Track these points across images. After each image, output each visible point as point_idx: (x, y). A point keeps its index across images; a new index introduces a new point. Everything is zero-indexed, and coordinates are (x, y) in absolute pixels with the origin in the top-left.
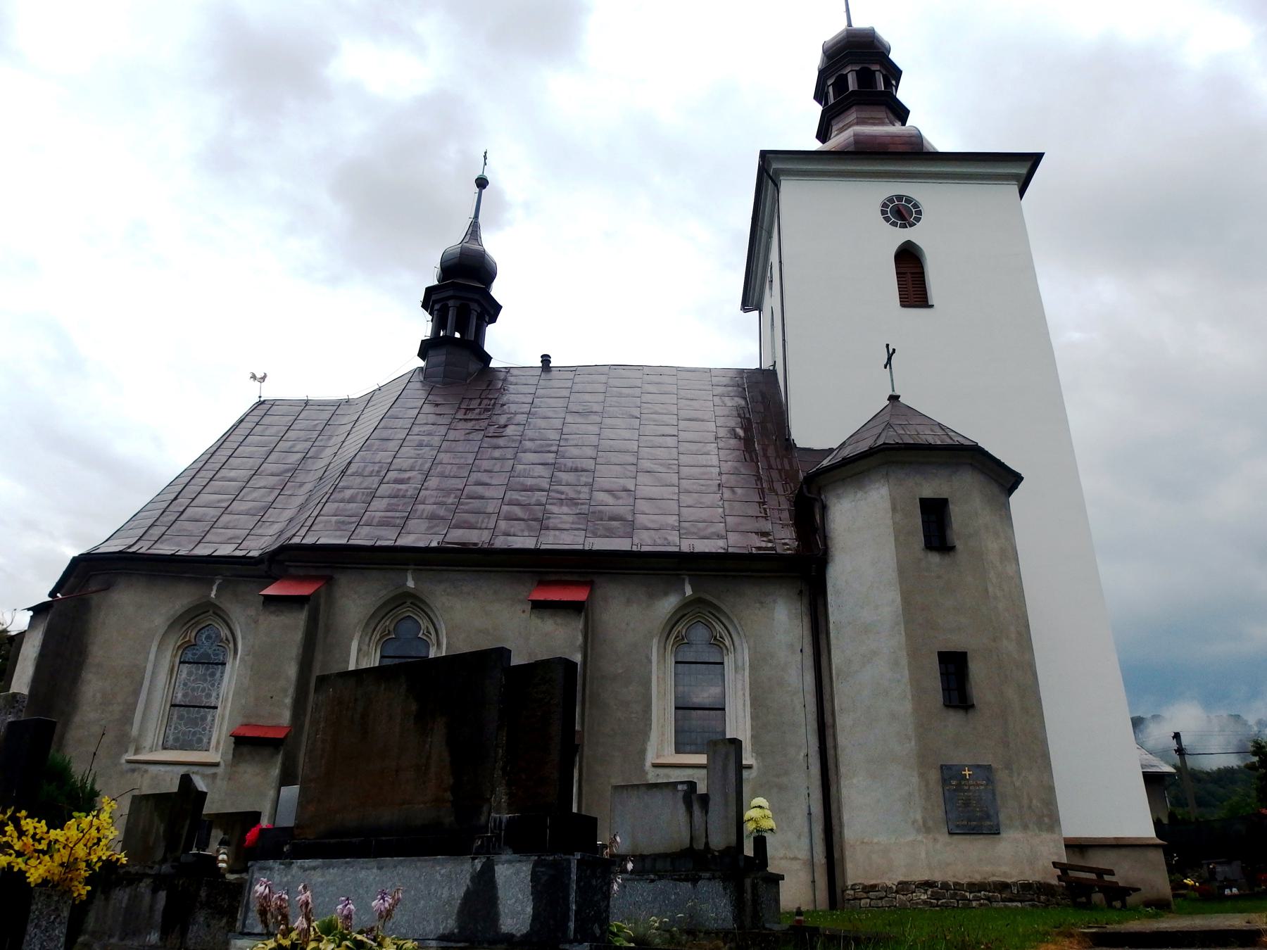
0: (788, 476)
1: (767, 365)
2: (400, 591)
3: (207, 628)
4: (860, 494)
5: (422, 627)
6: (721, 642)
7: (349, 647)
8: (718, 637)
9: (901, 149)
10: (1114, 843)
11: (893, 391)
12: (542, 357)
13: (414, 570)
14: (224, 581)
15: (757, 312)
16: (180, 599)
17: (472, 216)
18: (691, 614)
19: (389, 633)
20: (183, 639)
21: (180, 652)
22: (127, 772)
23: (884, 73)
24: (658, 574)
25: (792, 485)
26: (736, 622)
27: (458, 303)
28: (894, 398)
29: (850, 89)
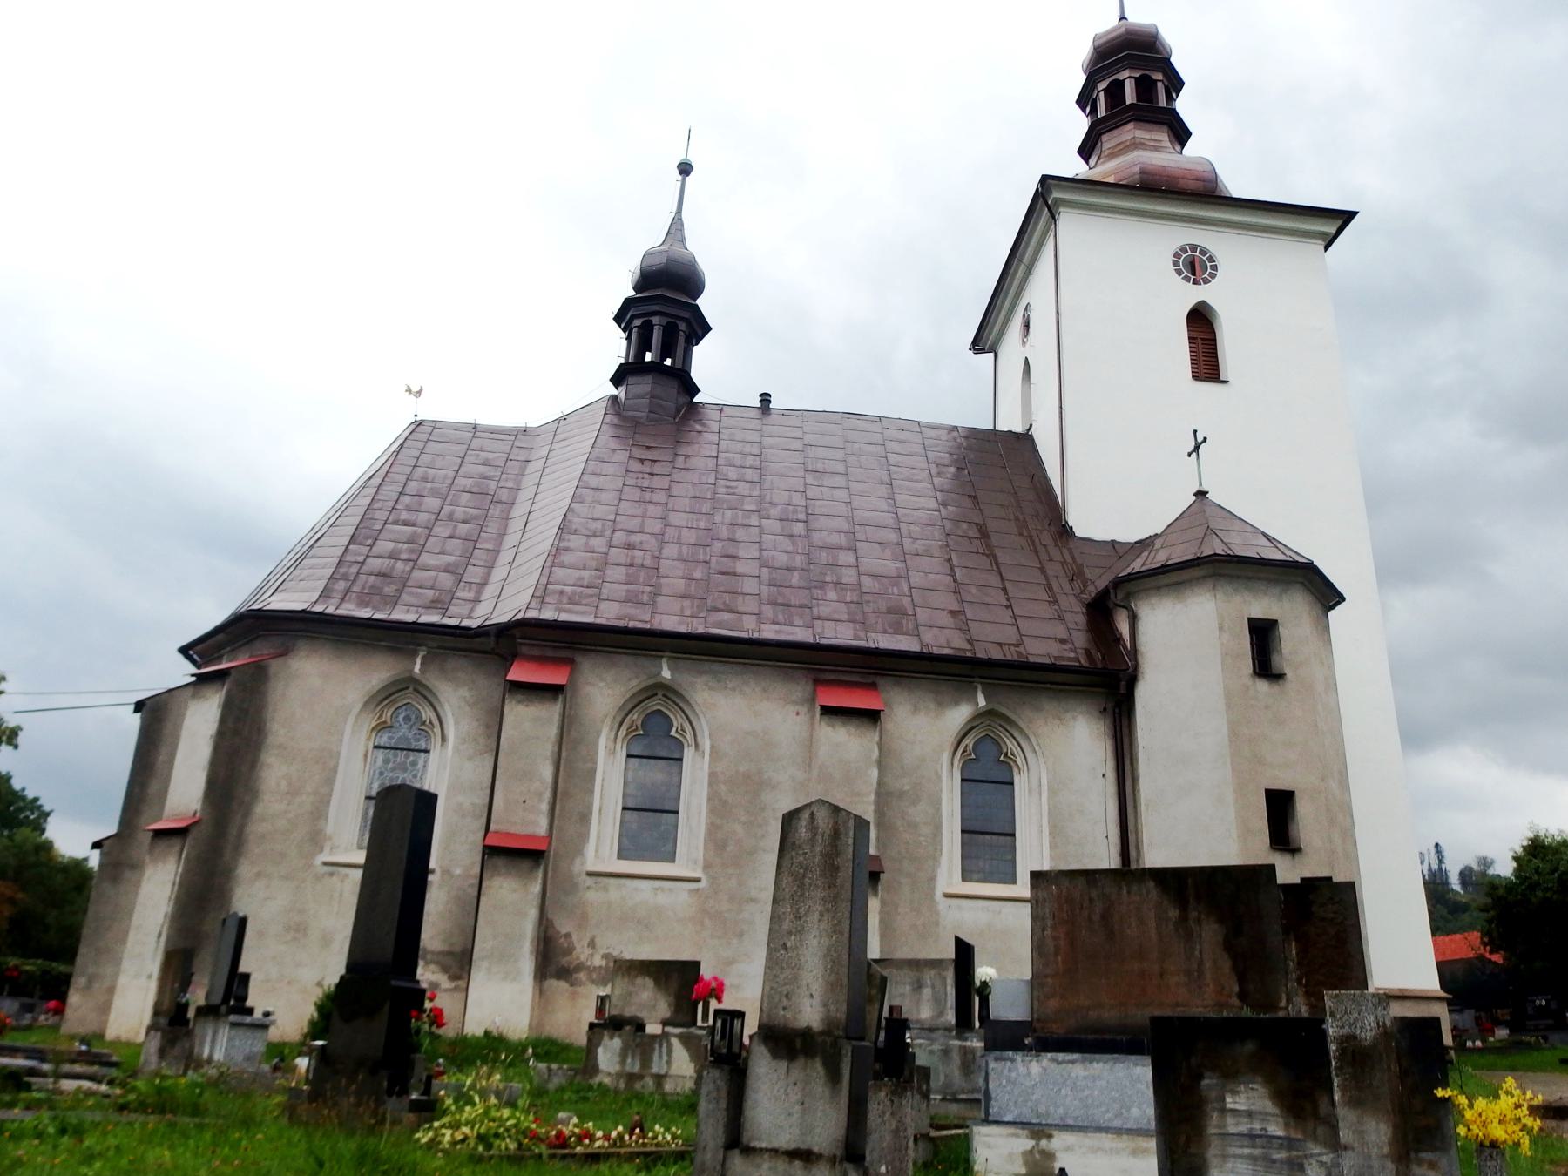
0: (1076, 575)
1: (1010, 422)
2: (652, 681)
3: (404, 708)
4: (1179, 606)
5: (675, 724)
6: (1011, 759)
7: (596, 744)
8: (1009, 754)
9: (1192, 185)
10: (1400, 994)
11: (1201, 484)
12: (761, 395)
13: (670, 658)
14: (428, 653)
15: (992, 354)
16: (376, 672)
17: (675, 210)
18: (980, 726)
19: (636, 730)
20: (379, 718)
21: (374, 735)
22: (323, 875)
23: (1166, 84)
24: (949, 680)
25: (1079, 581)
26: (1033, 739)
27: (665, 320)
28: (1201, 494)
29: (1128, 102)
